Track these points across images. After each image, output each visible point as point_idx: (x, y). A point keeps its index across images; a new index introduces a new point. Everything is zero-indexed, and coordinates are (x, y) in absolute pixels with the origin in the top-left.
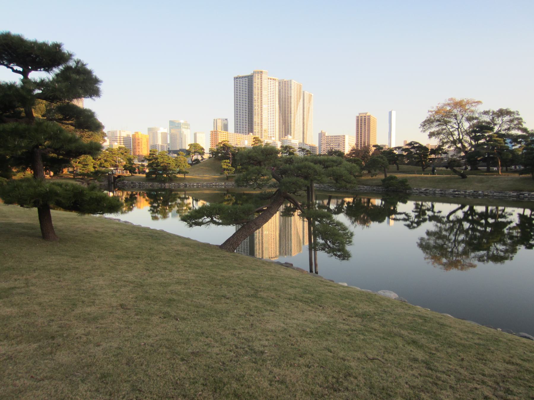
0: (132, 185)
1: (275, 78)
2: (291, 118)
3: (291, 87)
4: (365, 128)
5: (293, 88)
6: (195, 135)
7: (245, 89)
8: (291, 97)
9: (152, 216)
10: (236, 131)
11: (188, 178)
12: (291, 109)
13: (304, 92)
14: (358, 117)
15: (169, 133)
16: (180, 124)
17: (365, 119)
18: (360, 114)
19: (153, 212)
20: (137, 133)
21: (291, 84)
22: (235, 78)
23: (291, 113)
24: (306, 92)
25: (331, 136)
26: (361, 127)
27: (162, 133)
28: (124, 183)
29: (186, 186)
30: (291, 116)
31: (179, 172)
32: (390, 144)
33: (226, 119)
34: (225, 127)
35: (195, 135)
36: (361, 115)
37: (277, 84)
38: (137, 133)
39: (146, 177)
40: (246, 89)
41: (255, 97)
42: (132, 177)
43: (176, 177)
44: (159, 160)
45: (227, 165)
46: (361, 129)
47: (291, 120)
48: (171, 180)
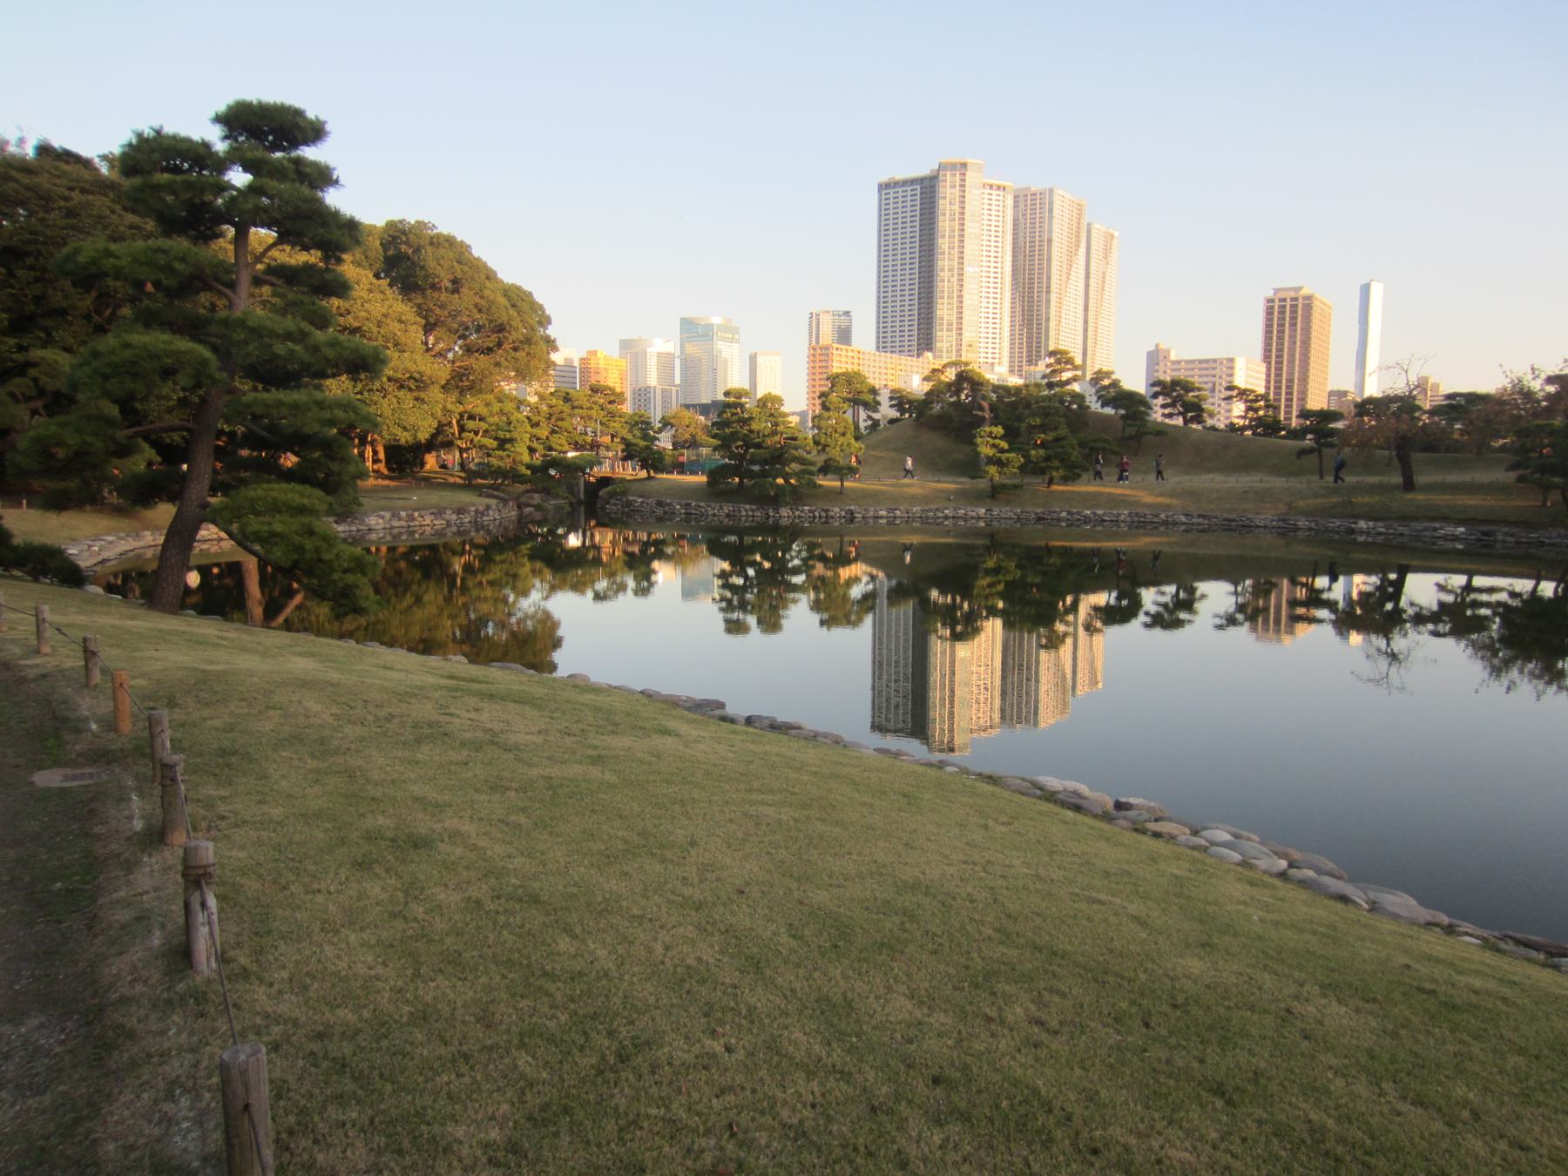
0: (659, 511)
2: (1048, 307)
3: (1051, 211)
4: (1293, 337)
5: (1056, 212)
6: (753, 359)
8: (1050, 241)
9: (727, 621)
10: (883, 345)
11: (853, 490)
12: (1049, 278)
13: (1089, 225)
14: (1270, 301)
15: (678, 353)
16: (710, 327)
17: (1294, 308)
18: (1277, 291)
19: (729, 607)
20: (594, 353)
21: (1051, 203)
23: (1048, 292)
24: (1095, 225)
25: (1188, 362)
26: (1281, 332)
27: (659, 355)
28: (629, 504)
29: (851, 517)
30: (1048, 301)
31: (825, 469)
32: (1361, 386)
33: (847, 313)
34: (844, 336)
35: (753, 359)
36: (1282, 295)
37: (1010, 202)
38: (594, 353)
39: (709, 483)
40: (915, 216)
41: (943, 243)
42: (651, 483)
43: (815, 485)
44: (754, 426)
45: (994, 446)
46: (1281, 338)
47: (1048, 314)
48: (796, 496)
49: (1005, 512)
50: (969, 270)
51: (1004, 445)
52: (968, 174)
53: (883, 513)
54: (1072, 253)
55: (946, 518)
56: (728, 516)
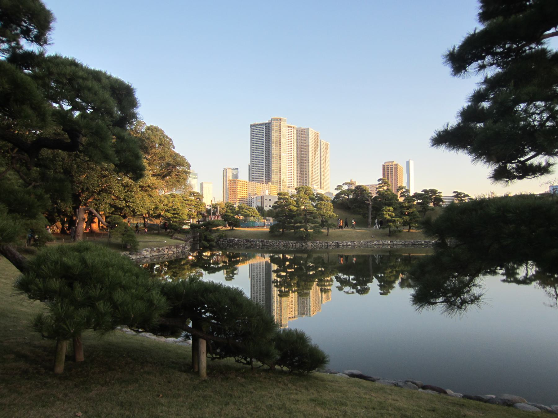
1: (293, 126)
2: (309, 167)
3: (308, 135)
4: (392, 178)
5: (310, 136)
6: (202, 185)
7: (262, 137)
8: (308, 145)
12: (309, 158)
14: (383, 166)
18: (385, 163)
21: (308, 133)
22: (251, 126)
23: (309, 162)
24: (322, 141)
30: (309, 165)
33: (237, 169)
35: (202, 185)
36: (387, 164)
37: (295, 132)
40: (263, 137)
41: (273, 145)
42: (233, 232)
47: (309, 169)
49: (398, 242)
50: (282, 155)
51: (394, 214)
52: (282, 122)
53: (349, 243)
54: (316, 150)
55: (375, 245)
56: (284, 246)
